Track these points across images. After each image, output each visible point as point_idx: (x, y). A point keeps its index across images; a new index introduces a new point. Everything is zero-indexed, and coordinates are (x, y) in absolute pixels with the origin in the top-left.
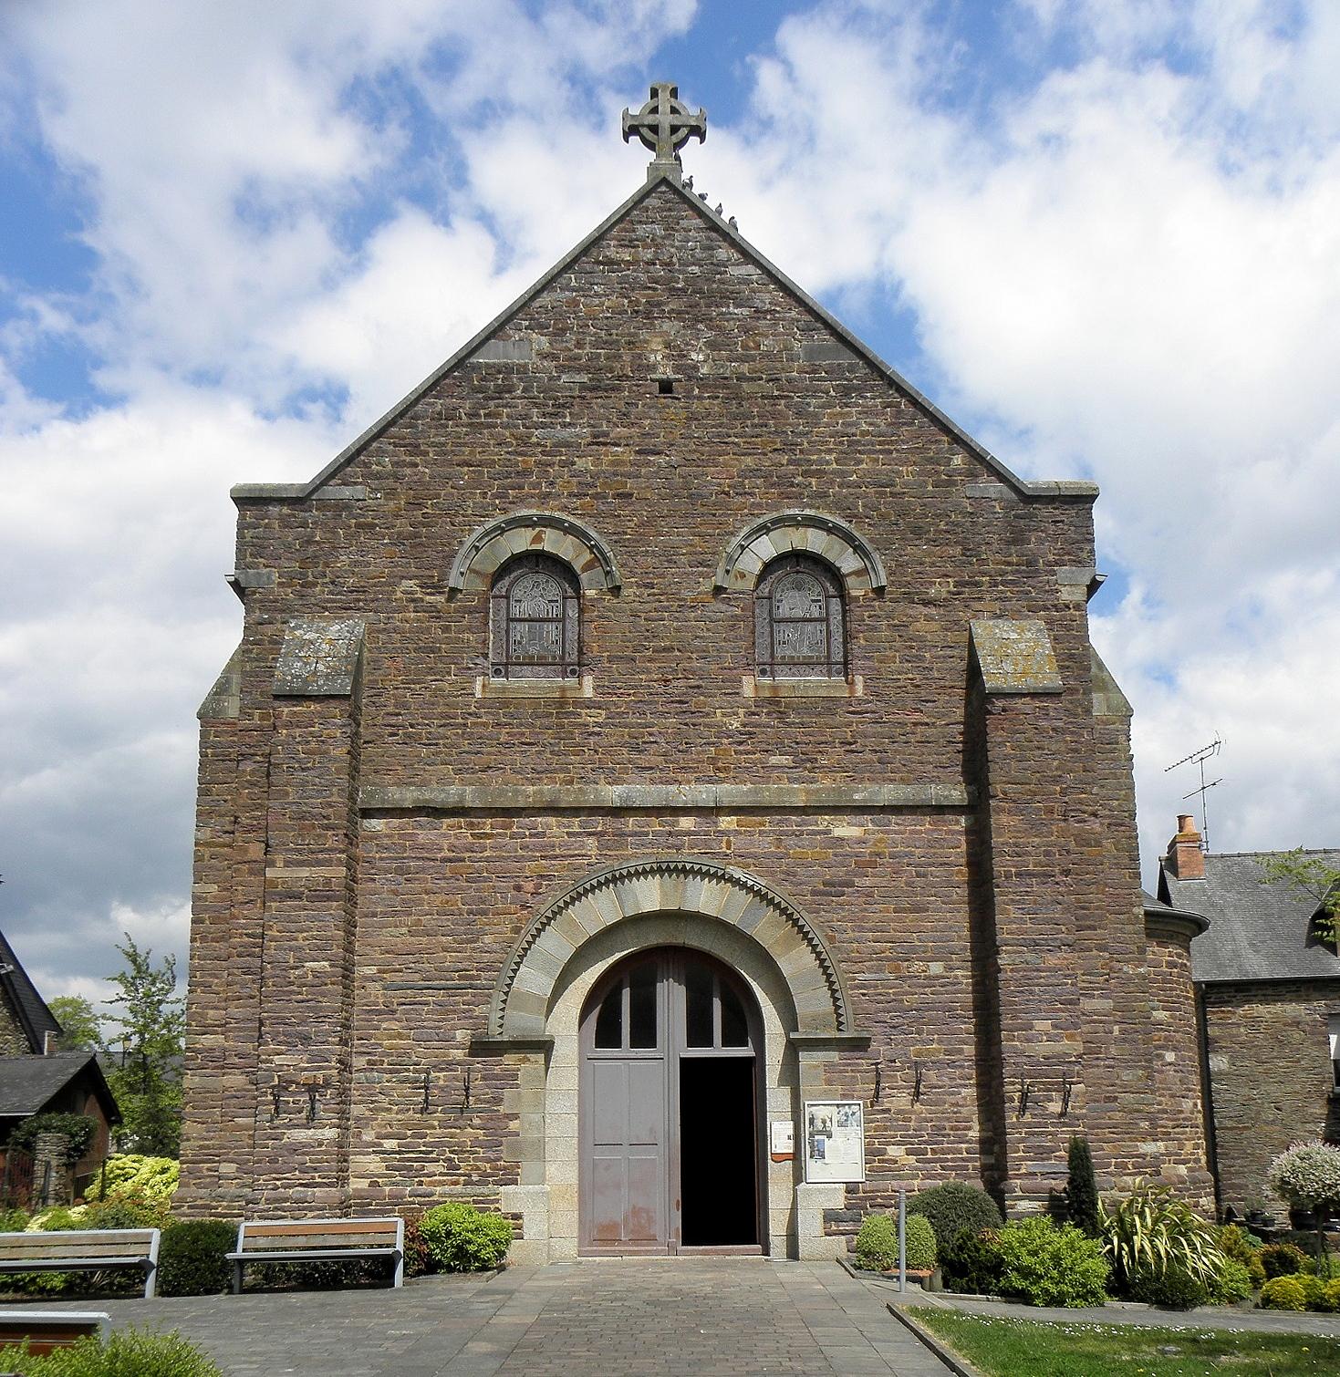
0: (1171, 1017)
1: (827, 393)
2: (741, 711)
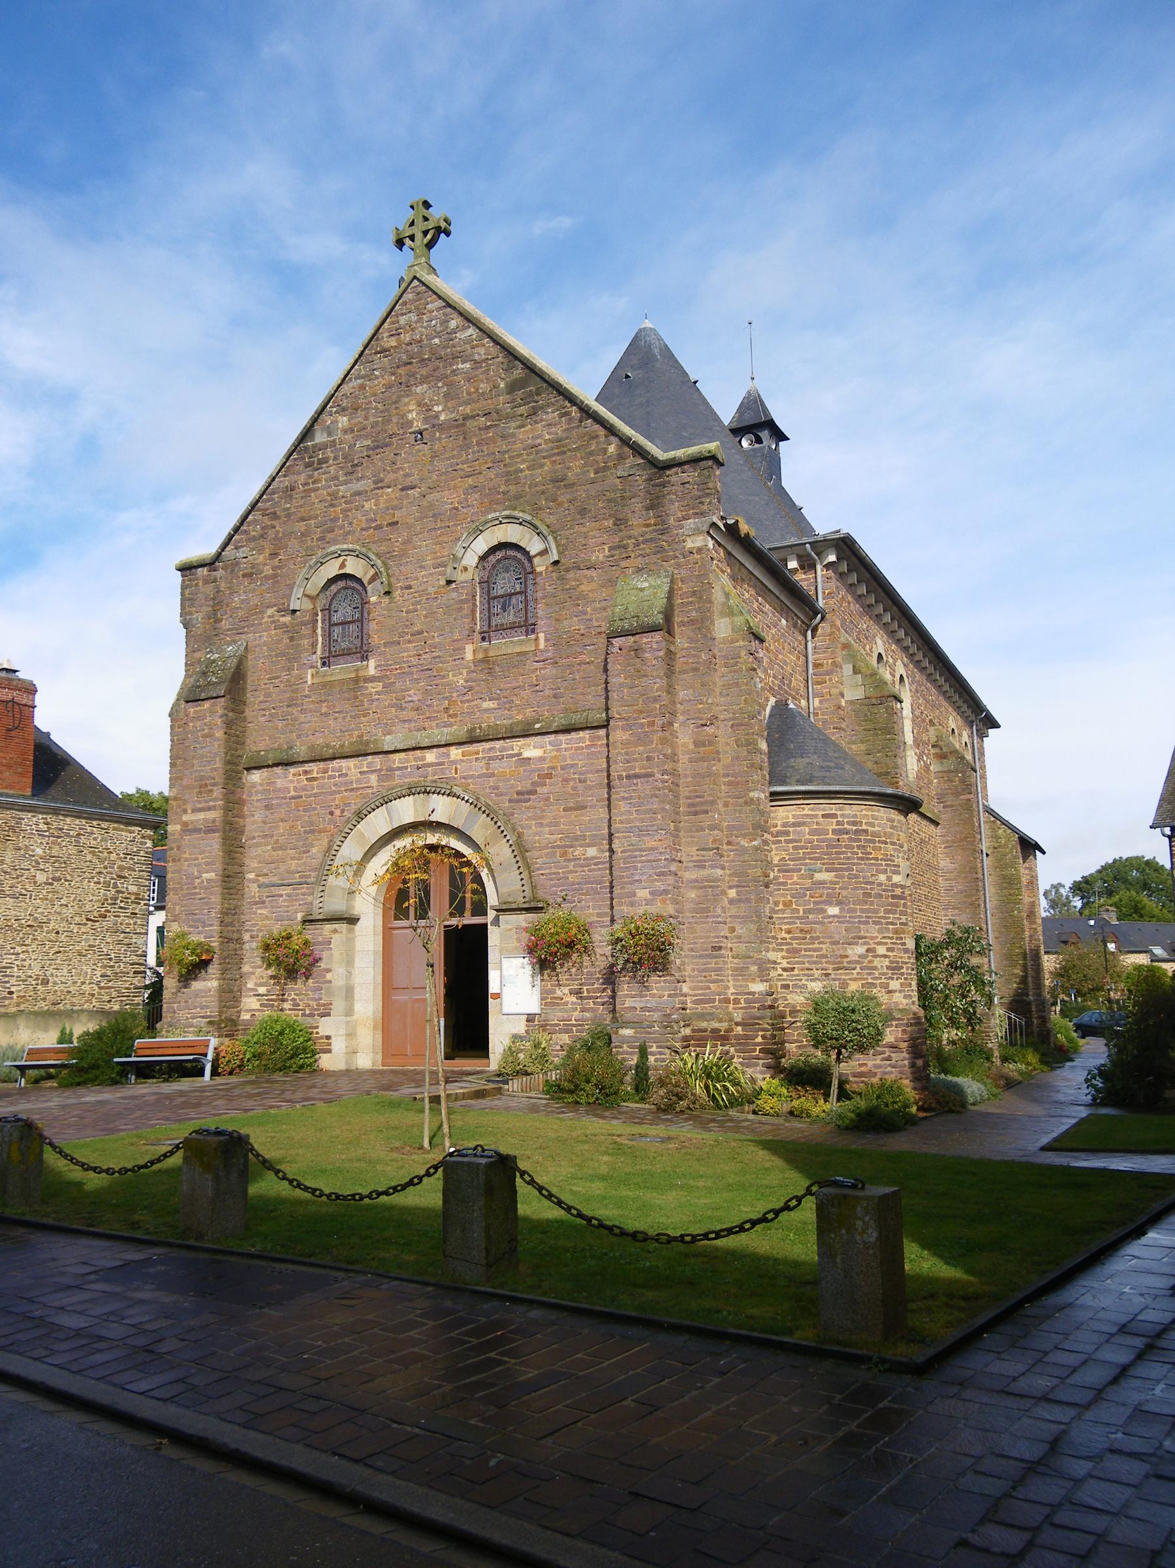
0: (836, 876)
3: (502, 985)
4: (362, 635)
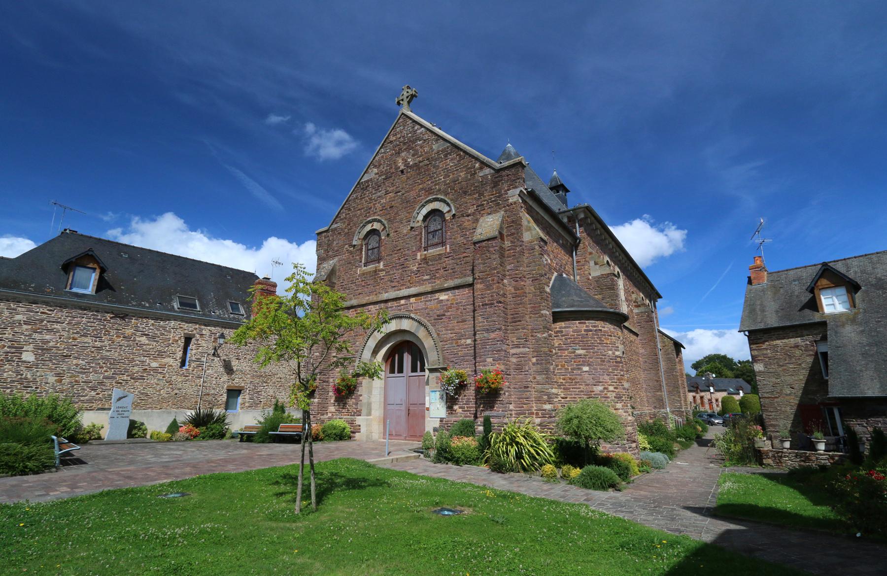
0: (587, 352)
3: (430, 403)
4: (379, 253)
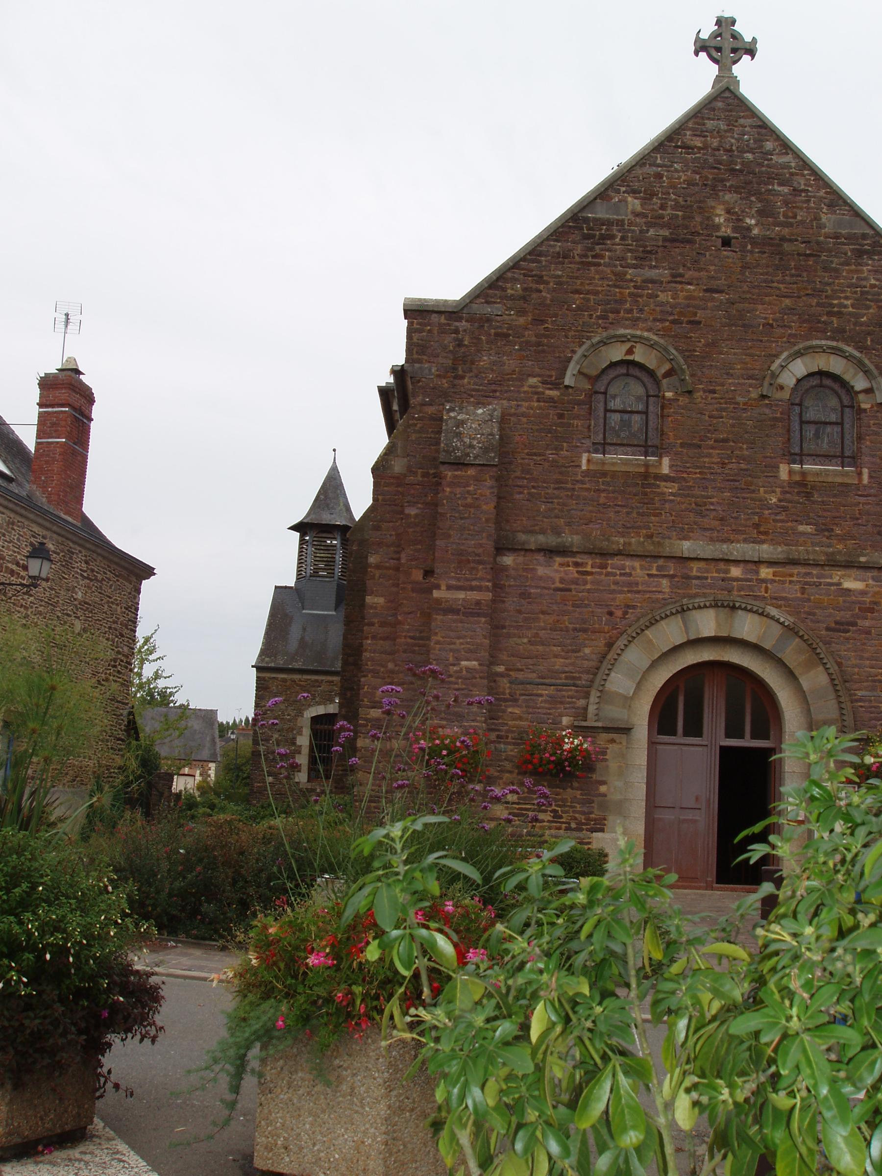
1: (846, 254)
2: (778, 490)
